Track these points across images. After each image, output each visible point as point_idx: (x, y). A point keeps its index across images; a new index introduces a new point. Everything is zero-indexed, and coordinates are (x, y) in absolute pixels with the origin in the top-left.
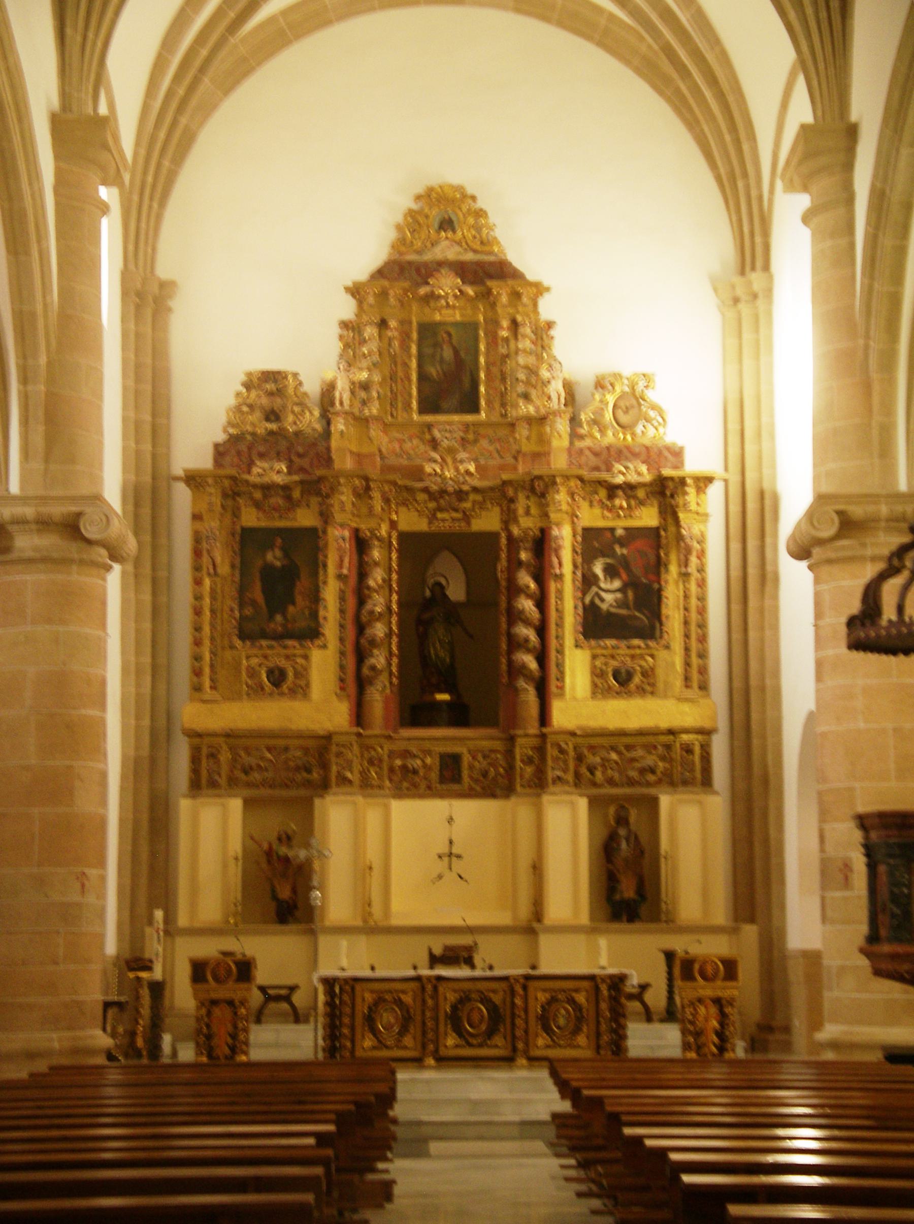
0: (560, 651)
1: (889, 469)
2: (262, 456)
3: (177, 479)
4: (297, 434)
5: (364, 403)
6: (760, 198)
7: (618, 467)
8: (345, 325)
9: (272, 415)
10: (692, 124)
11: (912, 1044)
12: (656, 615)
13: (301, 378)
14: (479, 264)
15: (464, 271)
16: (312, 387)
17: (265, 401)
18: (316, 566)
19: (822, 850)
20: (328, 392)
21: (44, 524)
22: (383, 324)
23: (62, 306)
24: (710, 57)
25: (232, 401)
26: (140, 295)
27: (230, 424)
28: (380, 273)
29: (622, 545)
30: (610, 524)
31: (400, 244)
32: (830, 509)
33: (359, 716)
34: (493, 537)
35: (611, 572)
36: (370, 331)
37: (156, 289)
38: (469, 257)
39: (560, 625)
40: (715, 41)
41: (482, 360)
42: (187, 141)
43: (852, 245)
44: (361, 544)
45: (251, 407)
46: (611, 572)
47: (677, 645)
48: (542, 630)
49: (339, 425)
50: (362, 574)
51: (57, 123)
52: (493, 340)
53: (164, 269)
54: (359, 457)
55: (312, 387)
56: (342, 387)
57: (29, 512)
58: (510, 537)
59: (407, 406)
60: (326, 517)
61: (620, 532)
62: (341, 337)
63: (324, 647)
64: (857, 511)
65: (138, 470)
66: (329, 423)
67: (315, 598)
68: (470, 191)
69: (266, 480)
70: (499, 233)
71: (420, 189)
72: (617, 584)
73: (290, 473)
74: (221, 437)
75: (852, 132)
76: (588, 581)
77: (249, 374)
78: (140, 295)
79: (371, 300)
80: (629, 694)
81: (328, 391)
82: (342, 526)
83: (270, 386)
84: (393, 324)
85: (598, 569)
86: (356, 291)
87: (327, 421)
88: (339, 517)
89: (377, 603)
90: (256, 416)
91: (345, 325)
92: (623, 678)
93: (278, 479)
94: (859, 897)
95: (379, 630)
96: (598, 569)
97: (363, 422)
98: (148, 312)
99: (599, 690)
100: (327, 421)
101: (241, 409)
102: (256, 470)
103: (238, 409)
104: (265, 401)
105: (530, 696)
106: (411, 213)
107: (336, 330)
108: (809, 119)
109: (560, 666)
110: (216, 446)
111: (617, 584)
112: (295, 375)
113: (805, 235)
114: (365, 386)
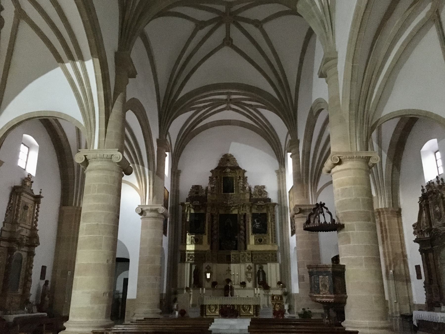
0: (249, 236)
1: (309, 201)
2: (195, 200)
3: (180, 204)
4: (201, 196)
5: (213, 191)
6: (283, 156)
7: (259, 202)
8: (210, 177)
9: (197, 193)
10: (270, 144)
11: (117, 1)
12: (266, 229)
13: (202, 186)
14: (234, 167)
15: (230, 168)
16: (204, 188)
17: (196, 191)
18: (204, 220)
19: (298, 274)
20: (207, 188)
21: (152, 211)
22: (217, 177)
23: (157, 171)
24: (273, 133)
25: (189, 190)
26: (174, 172)
27: (189, 194)
28: (216, 168)
29: (260, 216)
30: (258, 212)
31: (220, 164)
32: (298, 208)
33: (211, 248)
34: (236, 215)
35: (258, 221)
36: (214, 178)
37: (177, 172)
38: (232, 166)
39: (249, 231)
40: (274, 130)
41: (234, 183)
42: (184, 147)
43: (299, 161)
44: (212, 216)
45: (193, 191)
46: (258, 221)
47: (270, 235)
48: (245, 232)
49: (209, 194)
50: (213, 222)
51: (158, 141)
52: (236, 180)
53: (179, 168)
54: (212, 200)
55: (204, 188)
56: (209, 188)
57: (149, 208)
58: (239, 214)
59: (221, 191)
60: (206, 211)
61: (259, 214)
62: (209, 180)
63: (205, 235)
64: (303, 208)
65: (173, 203)
66: (207, 194)
67: (204, 226)
68: (232, 155)
69: (195, 204)
70: (238, 162)
71: (224, 154)
72: (259, 223)
73: (200, 203)
74: (188, 197)
75: (298, 142)
76: (253, 223)
77: (193, 186)
78: (174, 172)
79: (214, 173)
80: (262, 244)
81: (207, 188)
82: (209, 212)
83: (197, 188)
84: (219, 177)
85: (255, 221)
86: (212, 171)
87: (206, 193)
88: (208, 211)
89: (215, 227)
90: (194, 193)
91: (210, 177)
92: (260, 241)
93: (197, 204)
94: (84, 222)
95: (215, 232)
96: (255, 221)
97: (212, 194)
98: (176, 175)
99: (256, 243)
100: (206, 193)
101: (191, 192)
102: (194, 203)
103: (191, 192)
104: (196, 191)
105: (243, 244)
106: (222, 159)
107: (208, 178)
108: (290, 139)
109: (249, 238)
110: (187, 198)
111: (259, 223)
112: (201, 186)
113: (291, 159)
114: (213, 188)
